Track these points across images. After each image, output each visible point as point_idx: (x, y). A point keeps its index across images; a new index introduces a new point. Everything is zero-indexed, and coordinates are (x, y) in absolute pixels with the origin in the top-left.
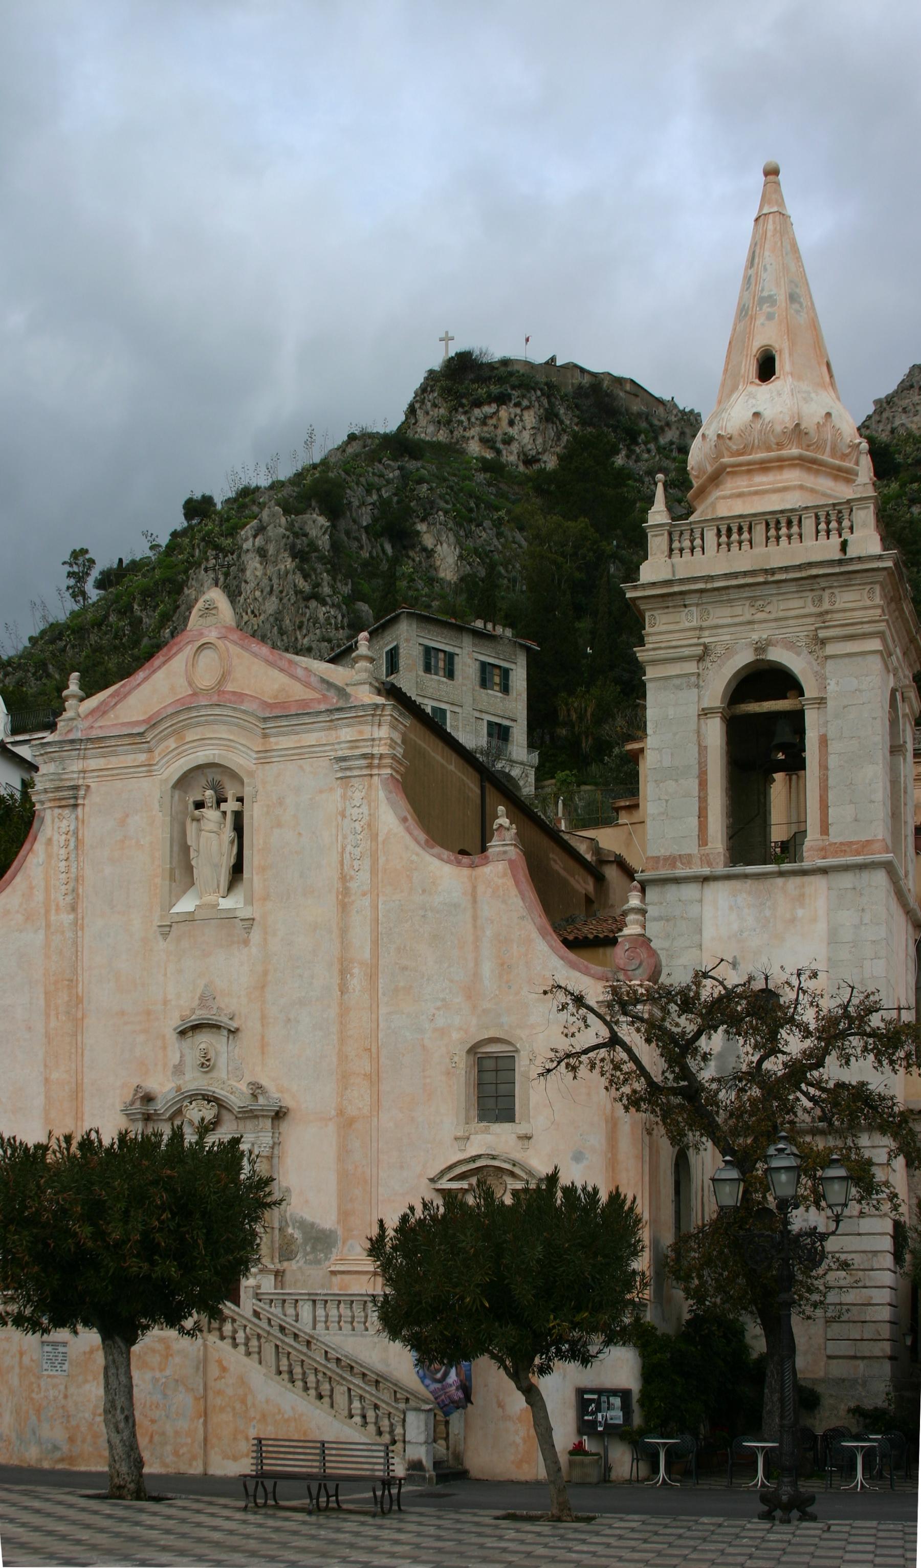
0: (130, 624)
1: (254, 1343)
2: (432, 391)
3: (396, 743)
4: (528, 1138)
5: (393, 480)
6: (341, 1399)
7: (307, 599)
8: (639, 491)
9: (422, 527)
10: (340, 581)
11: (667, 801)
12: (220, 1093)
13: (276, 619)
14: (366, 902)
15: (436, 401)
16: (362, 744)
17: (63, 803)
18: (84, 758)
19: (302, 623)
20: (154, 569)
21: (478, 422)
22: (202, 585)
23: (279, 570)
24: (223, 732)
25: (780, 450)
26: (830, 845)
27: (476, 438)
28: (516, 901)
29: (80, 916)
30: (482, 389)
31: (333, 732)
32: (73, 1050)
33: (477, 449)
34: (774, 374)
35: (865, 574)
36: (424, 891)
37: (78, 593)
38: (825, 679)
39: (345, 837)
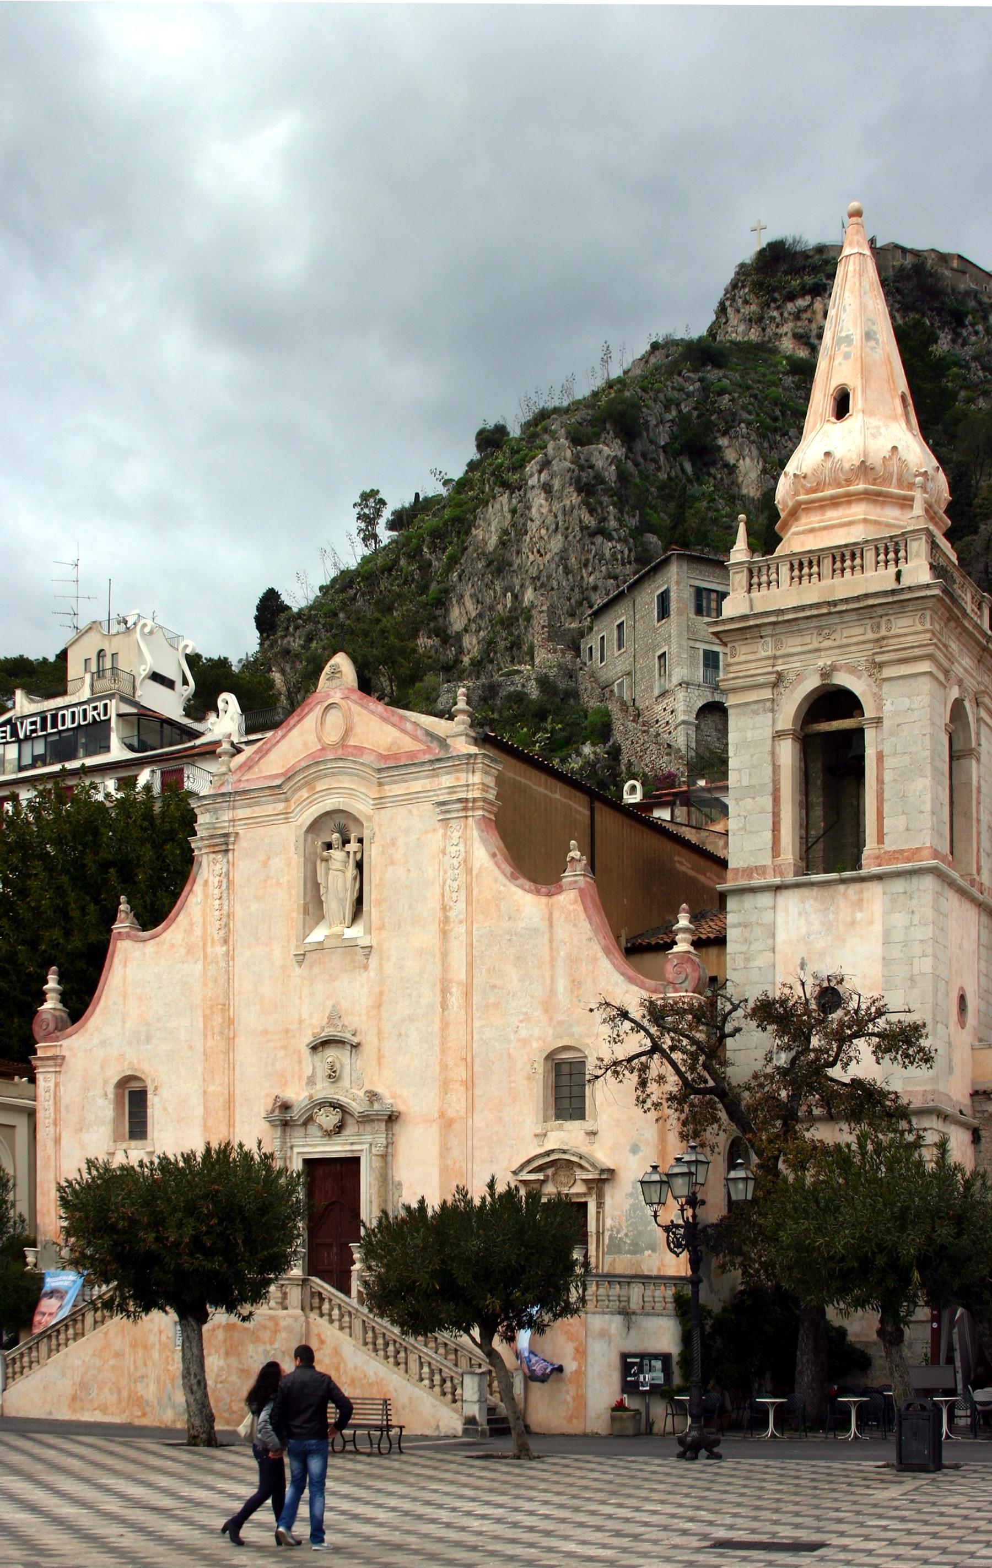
0: (419, 568)
1: (346, 1318)
2: (743, 287)
3: (488, 786)
4: (594, 1134)
5: (693, 393)
6: (414, 1366)
7: (593, 535)
8: (965, 379)
9: (723, 442)
10: (628, 513)
11: (745, 817)
12: (344, 1100)
13: (562, 558)
14: (462, 929)
15: (748, 297)
16: (459, 789)
17: (217, 849)
18: (234, 808)
19: (587, 560)
20: (444, 507)
21: (791, 317)
22: (489, 525)
23: (564, 506)
24: (346, 782)
25: (849, 486)
26: (885, 853)
27: (790, 335)
28: (585, 925)
29: (231, 948)
30: (796, 280)
31: (436, 779)
32: (226, 1066)
33: (791, 346)
34: (848, 411)
35: (915, 602)
36: (510, 918)
37: (369, 536)
38: (882, 700)
39: (445, 872)
